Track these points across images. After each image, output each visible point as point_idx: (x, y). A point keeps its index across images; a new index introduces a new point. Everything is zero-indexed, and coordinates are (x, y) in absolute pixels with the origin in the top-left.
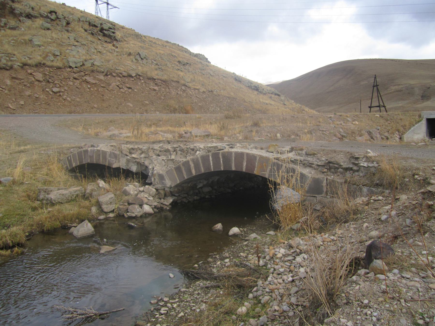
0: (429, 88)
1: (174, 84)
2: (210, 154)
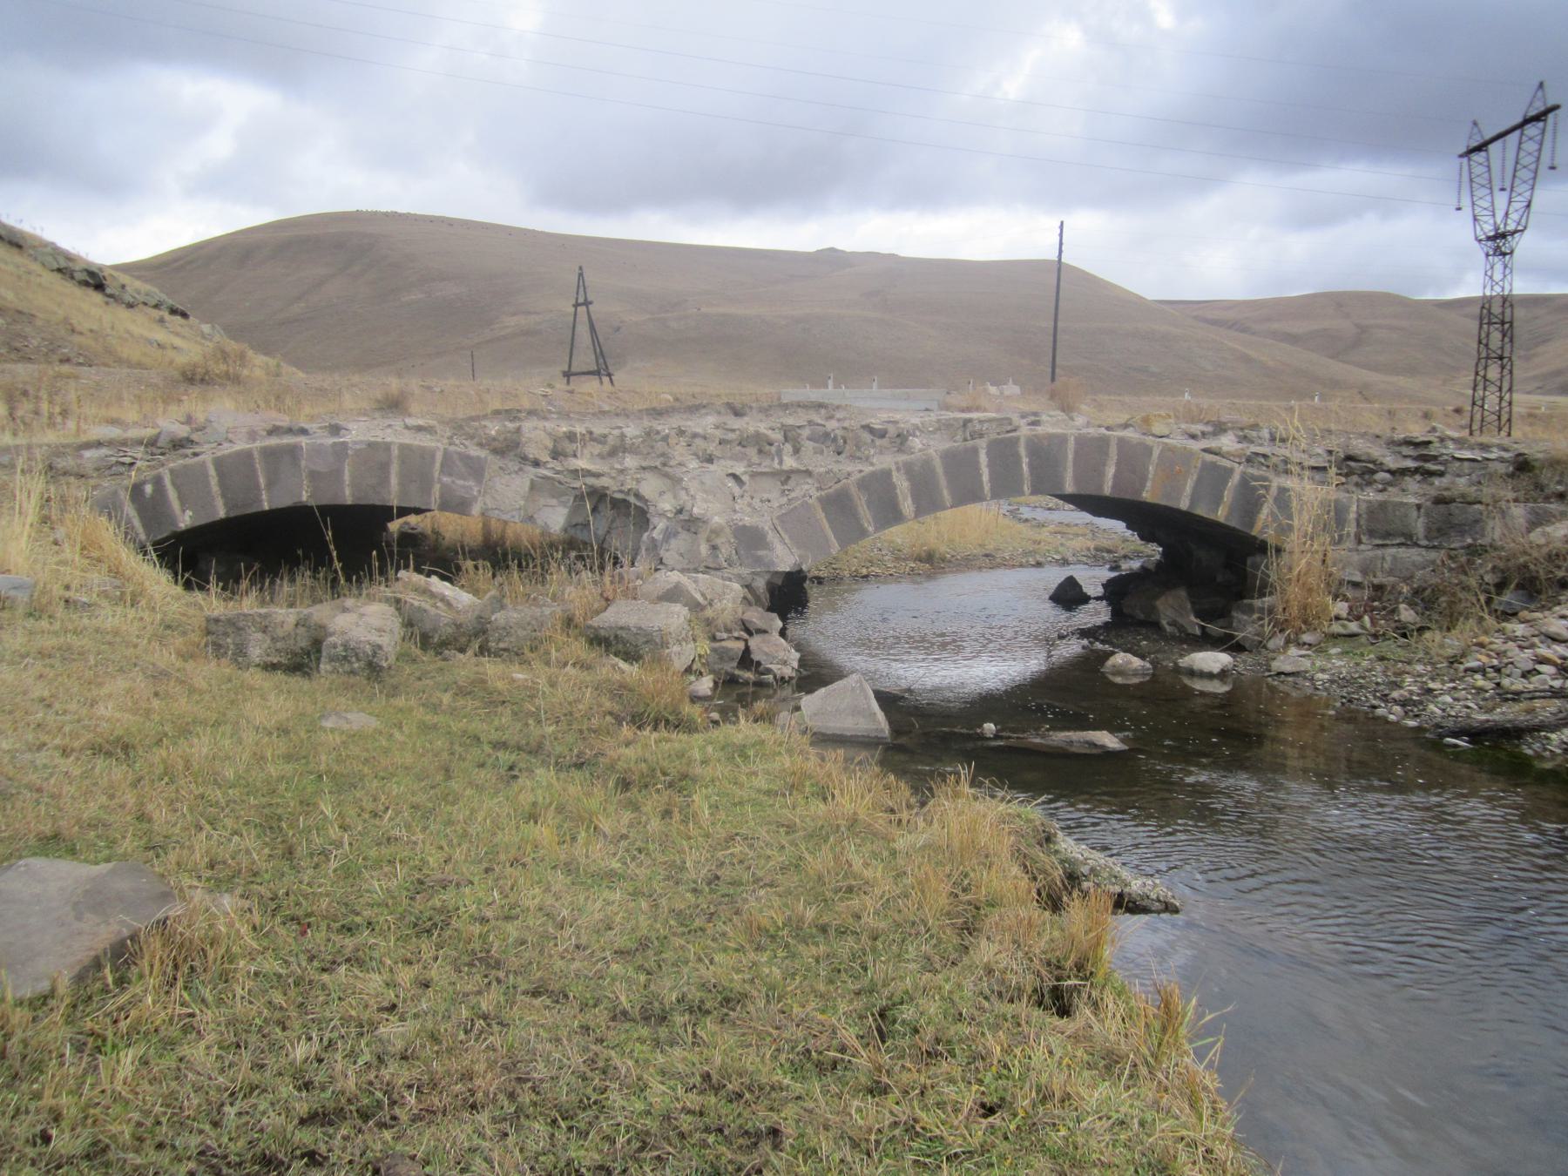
0: (618, 329)
2: (982, 444)
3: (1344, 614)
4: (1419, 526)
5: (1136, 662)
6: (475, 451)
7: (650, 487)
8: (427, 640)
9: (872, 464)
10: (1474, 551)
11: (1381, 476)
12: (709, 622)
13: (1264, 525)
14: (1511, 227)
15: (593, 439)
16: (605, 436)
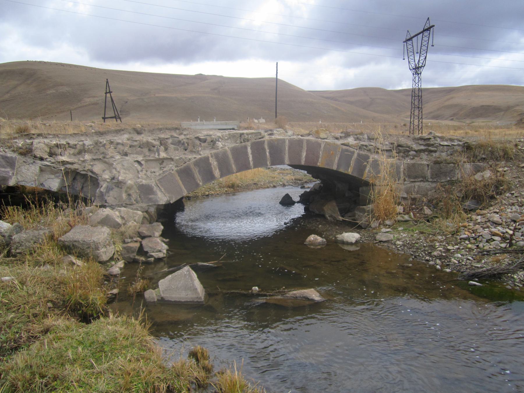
0: (127, 102)
2: (249, 144)
3: (402, 211)
4: (428, 174)
5: (319, 239)
6: (10, 154)
7: (98, 168)
9: (200, 155)
10: (452, 183)
11: (412, 153)
12: (122, 234)
13: (367, 175)
14: (420, 65)
16: (76, 145)
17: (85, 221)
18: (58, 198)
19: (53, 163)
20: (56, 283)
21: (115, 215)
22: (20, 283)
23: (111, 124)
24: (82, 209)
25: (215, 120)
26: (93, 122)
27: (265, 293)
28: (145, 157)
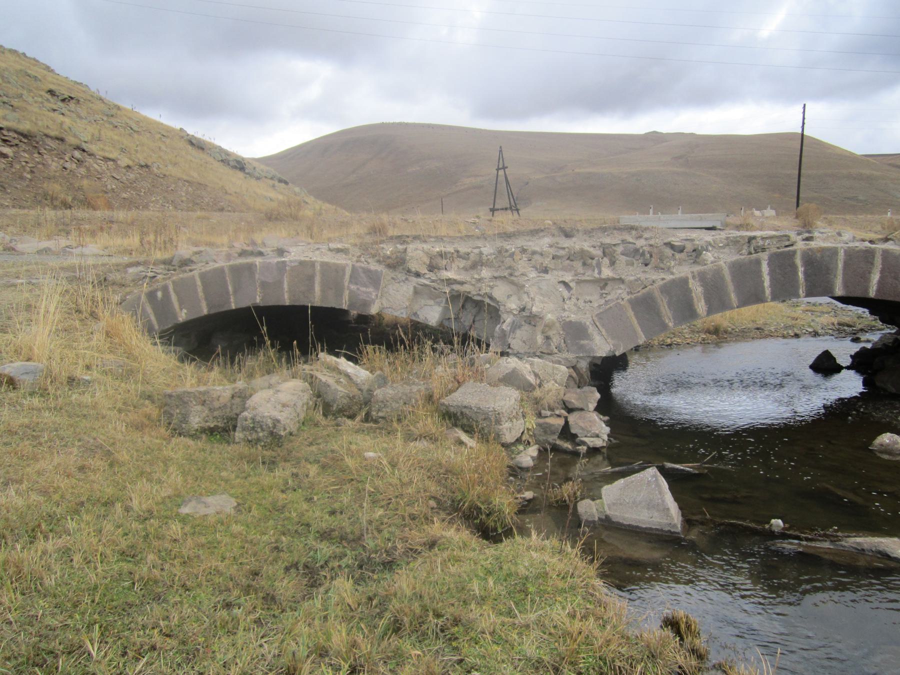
0: (527, 183)
1: (53, 144)
2: (764, 257)
6: (374, 266)
7: (500, 292)
8: (326, 406)
9: (672, 274)
12: (537, 401)
15: (459, 257)
16: (468, 254)
17: (479, 376)
18: (440, 336)
19: (433, 281)
20: (441, 471)
21: (524, 368)
22: (389, 463)
23: (505, 220)
24: (475, 356)
25: (680, 211)
26: (478, 217)
27: (797, 533)
28: (576, 275)
